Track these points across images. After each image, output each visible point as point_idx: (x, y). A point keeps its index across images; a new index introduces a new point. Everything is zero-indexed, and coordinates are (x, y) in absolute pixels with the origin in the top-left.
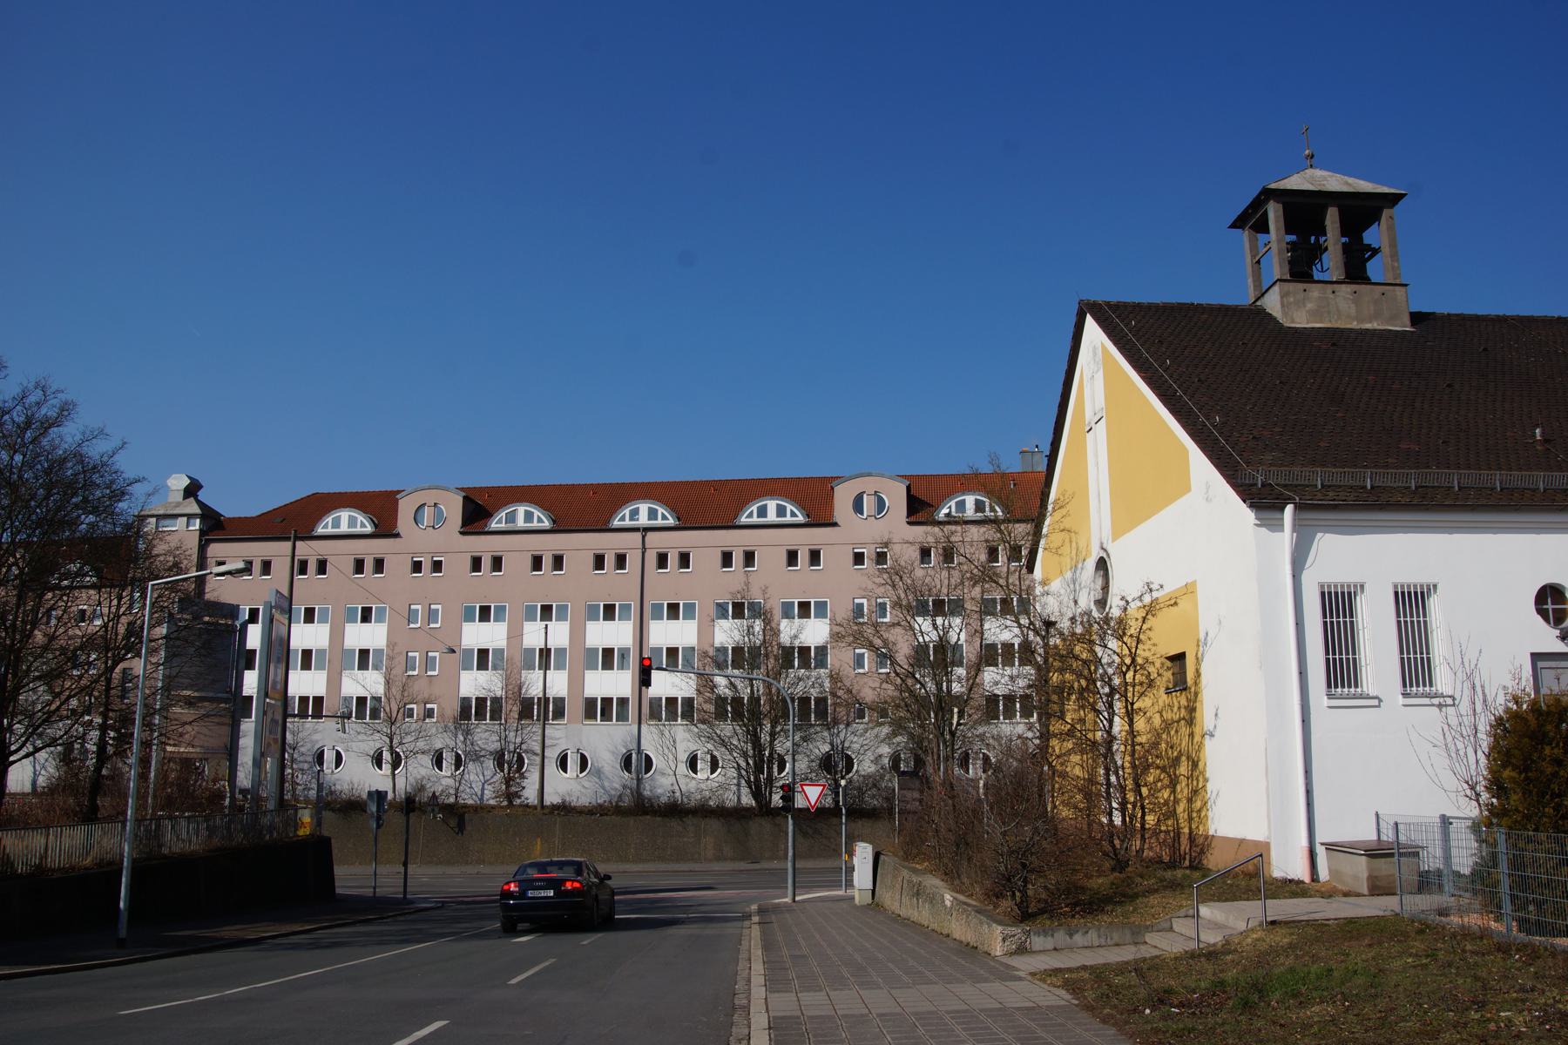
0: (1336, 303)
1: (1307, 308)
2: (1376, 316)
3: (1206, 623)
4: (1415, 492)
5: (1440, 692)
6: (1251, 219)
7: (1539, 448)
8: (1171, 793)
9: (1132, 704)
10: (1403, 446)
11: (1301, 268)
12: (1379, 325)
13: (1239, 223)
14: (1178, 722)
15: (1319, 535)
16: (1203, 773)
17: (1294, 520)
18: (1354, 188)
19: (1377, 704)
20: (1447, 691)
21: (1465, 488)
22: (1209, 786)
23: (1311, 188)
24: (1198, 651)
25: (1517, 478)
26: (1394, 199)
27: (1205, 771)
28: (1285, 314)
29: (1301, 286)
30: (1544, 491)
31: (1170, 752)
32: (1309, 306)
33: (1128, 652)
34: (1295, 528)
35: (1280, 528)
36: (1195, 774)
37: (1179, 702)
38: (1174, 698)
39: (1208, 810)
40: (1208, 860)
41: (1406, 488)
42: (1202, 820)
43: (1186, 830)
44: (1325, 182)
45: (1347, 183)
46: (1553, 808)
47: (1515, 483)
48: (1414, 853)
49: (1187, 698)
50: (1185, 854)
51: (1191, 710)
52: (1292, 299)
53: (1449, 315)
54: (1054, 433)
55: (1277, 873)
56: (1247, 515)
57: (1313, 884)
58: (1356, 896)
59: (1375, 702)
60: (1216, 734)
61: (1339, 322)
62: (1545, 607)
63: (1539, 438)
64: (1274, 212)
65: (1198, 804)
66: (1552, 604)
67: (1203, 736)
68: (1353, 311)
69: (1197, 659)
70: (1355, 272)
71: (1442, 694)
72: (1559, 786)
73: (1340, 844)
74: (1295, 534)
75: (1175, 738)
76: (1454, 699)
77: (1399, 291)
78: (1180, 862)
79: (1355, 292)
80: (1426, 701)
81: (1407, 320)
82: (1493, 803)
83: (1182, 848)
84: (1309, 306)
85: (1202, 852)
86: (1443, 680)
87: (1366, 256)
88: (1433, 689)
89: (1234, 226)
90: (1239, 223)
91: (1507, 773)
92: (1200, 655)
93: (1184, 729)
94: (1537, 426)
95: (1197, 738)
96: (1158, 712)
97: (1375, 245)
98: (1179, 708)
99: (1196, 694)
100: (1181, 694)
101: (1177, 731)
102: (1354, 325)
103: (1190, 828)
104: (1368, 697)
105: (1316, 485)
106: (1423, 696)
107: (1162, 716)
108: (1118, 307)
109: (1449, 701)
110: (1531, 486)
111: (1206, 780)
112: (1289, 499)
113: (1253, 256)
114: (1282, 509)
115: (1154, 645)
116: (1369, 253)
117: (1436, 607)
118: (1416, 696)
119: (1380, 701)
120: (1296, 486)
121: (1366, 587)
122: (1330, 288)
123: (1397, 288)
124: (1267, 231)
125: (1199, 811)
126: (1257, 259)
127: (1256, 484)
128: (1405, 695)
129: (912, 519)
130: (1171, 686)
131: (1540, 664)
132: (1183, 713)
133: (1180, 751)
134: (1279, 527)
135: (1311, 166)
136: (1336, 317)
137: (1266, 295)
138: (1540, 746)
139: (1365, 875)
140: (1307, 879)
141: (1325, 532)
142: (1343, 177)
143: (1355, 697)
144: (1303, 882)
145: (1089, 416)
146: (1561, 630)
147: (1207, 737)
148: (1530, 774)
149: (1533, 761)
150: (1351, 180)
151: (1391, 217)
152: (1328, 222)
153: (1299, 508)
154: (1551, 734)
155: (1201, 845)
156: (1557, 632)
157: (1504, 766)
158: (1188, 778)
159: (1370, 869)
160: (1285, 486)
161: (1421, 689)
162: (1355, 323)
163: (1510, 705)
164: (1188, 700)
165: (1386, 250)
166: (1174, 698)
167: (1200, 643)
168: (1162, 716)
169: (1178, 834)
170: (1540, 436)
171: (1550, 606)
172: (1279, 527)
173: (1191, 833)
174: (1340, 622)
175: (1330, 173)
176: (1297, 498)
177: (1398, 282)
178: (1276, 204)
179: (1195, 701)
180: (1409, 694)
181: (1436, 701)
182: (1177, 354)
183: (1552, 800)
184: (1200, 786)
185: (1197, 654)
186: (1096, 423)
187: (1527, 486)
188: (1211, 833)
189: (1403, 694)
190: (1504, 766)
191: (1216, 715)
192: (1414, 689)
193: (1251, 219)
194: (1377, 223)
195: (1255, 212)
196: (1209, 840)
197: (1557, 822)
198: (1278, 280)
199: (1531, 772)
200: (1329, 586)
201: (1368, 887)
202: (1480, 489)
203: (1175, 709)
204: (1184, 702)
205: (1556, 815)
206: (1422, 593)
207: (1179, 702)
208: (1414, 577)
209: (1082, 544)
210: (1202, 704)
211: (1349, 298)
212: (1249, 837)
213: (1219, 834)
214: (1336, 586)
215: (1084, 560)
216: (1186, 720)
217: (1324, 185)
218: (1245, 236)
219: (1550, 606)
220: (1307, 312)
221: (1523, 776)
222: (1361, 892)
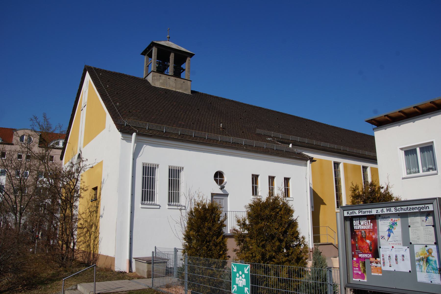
0: (169, 82)
1: (160, 82)
2: (181, 88)
3: (104, 176)
4: (179, 136)
5: (181, 205)
6: (147, 52)
7: (221, 130)
8: (89, 238)
9: (72, 203)
10: (179, 122)
11: (161, 69)
12: (181, 91)
13: (144, 53)
14: (93, 212)
15: (145, 146)
16: (98, 231)
17: (136, 139)
18: (180, 49)
19: (159, 208)
20: (183, 204)
21: (196, 137)
22: (100, 236)
23: (167, 45)
24: (101, 186)
25: (213, 136)
26: (191, 55)
27: (99, 230)
28: (153, 82)
29: (159, 74)
30: (220, 141)
31: (90, 223)
32: (161, 81)
33: (72, 184)
34: (135, 142)
36: (96, 231)
37: (94, 205)
38: (93, 203)
39: (99, 244)
40: (97, 263)
41: (177, 134)
42: (97, 248)
43: (92, 252)
44: (172, 45)
45: (178, 47)
46: (206, 247)
47: (213, 138)
48: (165, 261)
49: (96, 203)
50: (92, 261)
51: (97, 207)
52: (156, 78)
53: (202, 93)
54: (73, 111)
55: (117, 269)
56: (119, 135)
57: (130, 273)
58: (142, 278)
59: (158, 207)
60: (103, 216)
61: (169, 88)
62: (217, 178)
63: (221, 127)
64: (154, 50)
65: (96, 242)
66: (219, 178)
67: (99, 217)
68: (174, 85)
69: (100, 189)
70: (178, 73)
71: (182, 205)
72: (209, 238)
73: (139, 259)
74: (135, 144)
75: (92, 218)
76: (185, 207)
77: (189, 82)
78: (90, 264)
79: (176, 80)
80: (176, 207)
81: (190, 92)
82: (186, 245)
83: (91, 258)
85: (96, 260)
86: (183, 201)
87: (181, 71)
88: (179, 203)
89: (142, 54)
90: (144, 53)
91: (191, 233)
92: (101, 188)
93: (95, 214)
95: (98, 218)
96: (88, 208)
97: (184, 68)
98: (94, 207)
99: (99, 201)
100: (95, 202)
101: (93, 215)
102: (174, 90)
103: (93, 251)
104: (156, 205)
105: (146, 128)
106: (175, 205)
107: (89, 210)
108: (99, 71)
109: (184, 208)
110: (216, 139)
111: (99, 233)
112: (135, 131)
113: (147, 64)
114: (132, 134)
115: (84, 182)
116: (182, 70)
117: (183, 175)
118: (173, 205)
119: (160, 206)
120: (139, 128)
121: (159, 166)
122: (168, 77)
123: (188, 81)
124: (151, 58)
125: (96, 245)
127: (124, 125)
128: (169, 205)
129: (40, 146)
130: (93, 199)
131: (214, 197)
132: (95, 208)
133: (93, 222)
134: (130, 141)
135: (169, 40)
136: (169, 86)
137: (148, 76)
138: (204, 222)
139: (146, 270)
140: (128, 272)
141: (147, 145)
142: (177, 45)
143: (151, 205)
144: (126, 273)
146: (221, 186)
147: (101, 217)
148: (199, 233)
149: (201, 228)
150: (179, 47)
151: (189, 60)
152: (171, 57)
153: (138, 134)
154: (208, 218)
155: (96, 257)
156: (220, 187)
157: (191, 230)
158: (94, 233)
159: (148, 268)
160: (135, 127)
161: (175, 203)
162: (174, 89)
163: (196, 206)
164: (97, 204)
165: (187, 70)
166: (93, 203)
167: (102, 183)
168: (89, 210)
169: (90, 253)
170: (222, 126)
171: (218, 178)
172: (130, 141)
173: (94, 253)
174: (172, 192)
175: (174, 44)
176: (137, 131)
177: (189, 79)
178: (155, 47)
179: (98, 204)
180: (171, 205)
181: (179, 208)
182: (113, 85)
183: (206, 243)
184: (97, 236)
185: (100, 187)
186: (84, 107)
187: (215, 139)
188: (99, 253)
189: (168, 204)
190: (191, 230)
191: (104, 209)
192: (172, 203)
193: (147, 52)
195: (149, 50)
196: (98, 256)
197: (207, 252)
198: (152, 71)
199: (200, 232)
200: (146, 164)
201: (147, 275)
202: (201, 138)
203: (93, 207)
204: (95, 205)
205: (207, 249)
206: (178, 170)
207: (94, 205)
208: (176, 164)
209: (75, 150)
210: (100, 205)
211: (173, 81)
212: (109, 255)
213: (101, 254)
214: (148, 164)
215: (75, 155)
216: (95, 212)
217: (171, 46)
218: (145, 57)
219: (218, 178)
221: (197, 234)
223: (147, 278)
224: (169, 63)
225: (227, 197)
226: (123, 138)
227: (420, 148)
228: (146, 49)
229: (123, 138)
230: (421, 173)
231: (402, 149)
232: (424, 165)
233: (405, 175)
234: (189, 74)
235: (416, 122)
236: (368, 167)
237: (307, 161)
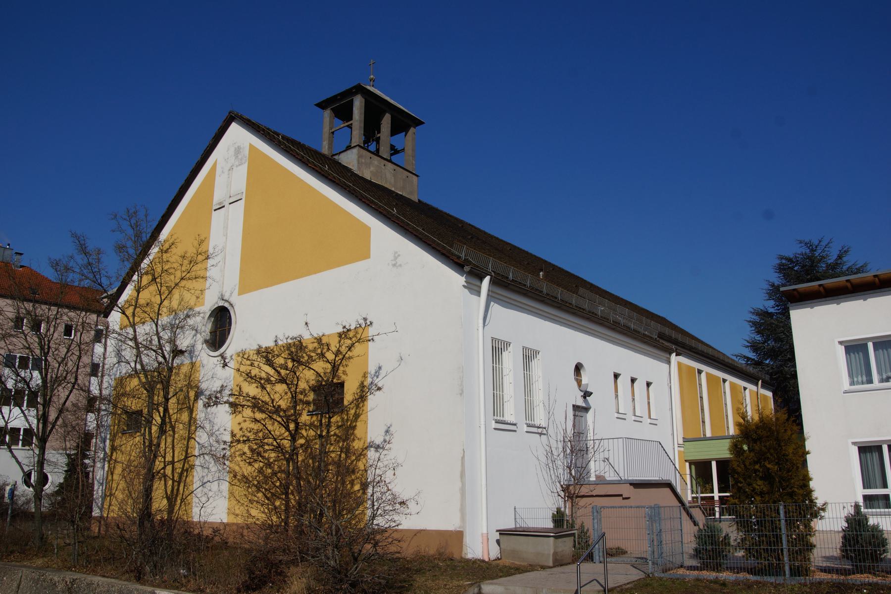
26: (418, 123)
28: (359, 168)
32: (372, 169)
35: (478, 293)
84: (372, 169)
94: (542, 270)
102: (393, 189)
113: (331, 128)
114: (481, 279)
126: (333, 130)
135: (373, 86)
139: (552, 552)
145: (219, 195)
153: (493, 282)
181: (540, 430)
186: (230, 204)
194: (404, 133)
220: (371, 172)
222: (546, 564)
223: (554, 567)
224: (379, 132)
225: (587, 413)
226: (466, 284)
227: (874, 344)
228: (335, 96)
229: (466, 284)
230: (876, 383)
231: (841, 343)
232: (880, 372)
233: (846, 385)
234: (414, 162)
235: (869, 300)
236: (703, 371)
237: (670, 355)
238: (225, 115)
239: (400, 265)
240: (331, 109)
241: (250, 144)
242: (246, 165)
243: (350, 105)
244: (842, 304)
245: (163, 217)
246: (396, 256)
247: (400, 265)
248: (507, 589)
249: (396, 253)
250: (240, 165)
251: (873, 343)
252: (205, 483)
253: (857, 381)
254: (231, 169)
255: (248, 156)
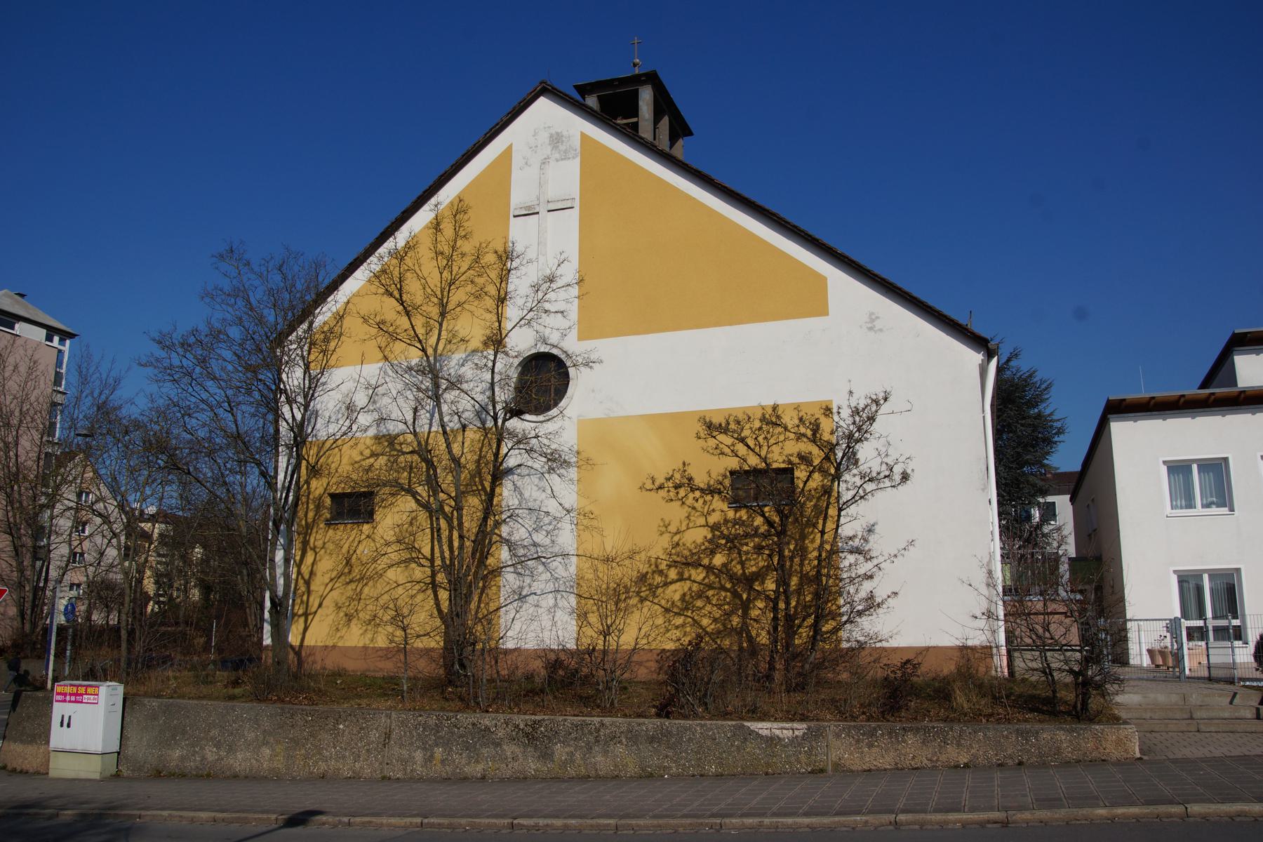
186: (549, 211)
238: (534, 84)
239: (881, 330)
240: (598, 96)
241: (581, 132)
242: (578, 159)
243: (635, 97)
244: (1169, 421)
245: (404, 212)
246: (873, 318)
247: (881, 330)
248: (1145, 697)
249: (872, 314)
250: (562, 159)
251: (1198, 465)
252: (525, 597)
253: (1176, 505)
254: (545, 162)
255: (579, 149)
